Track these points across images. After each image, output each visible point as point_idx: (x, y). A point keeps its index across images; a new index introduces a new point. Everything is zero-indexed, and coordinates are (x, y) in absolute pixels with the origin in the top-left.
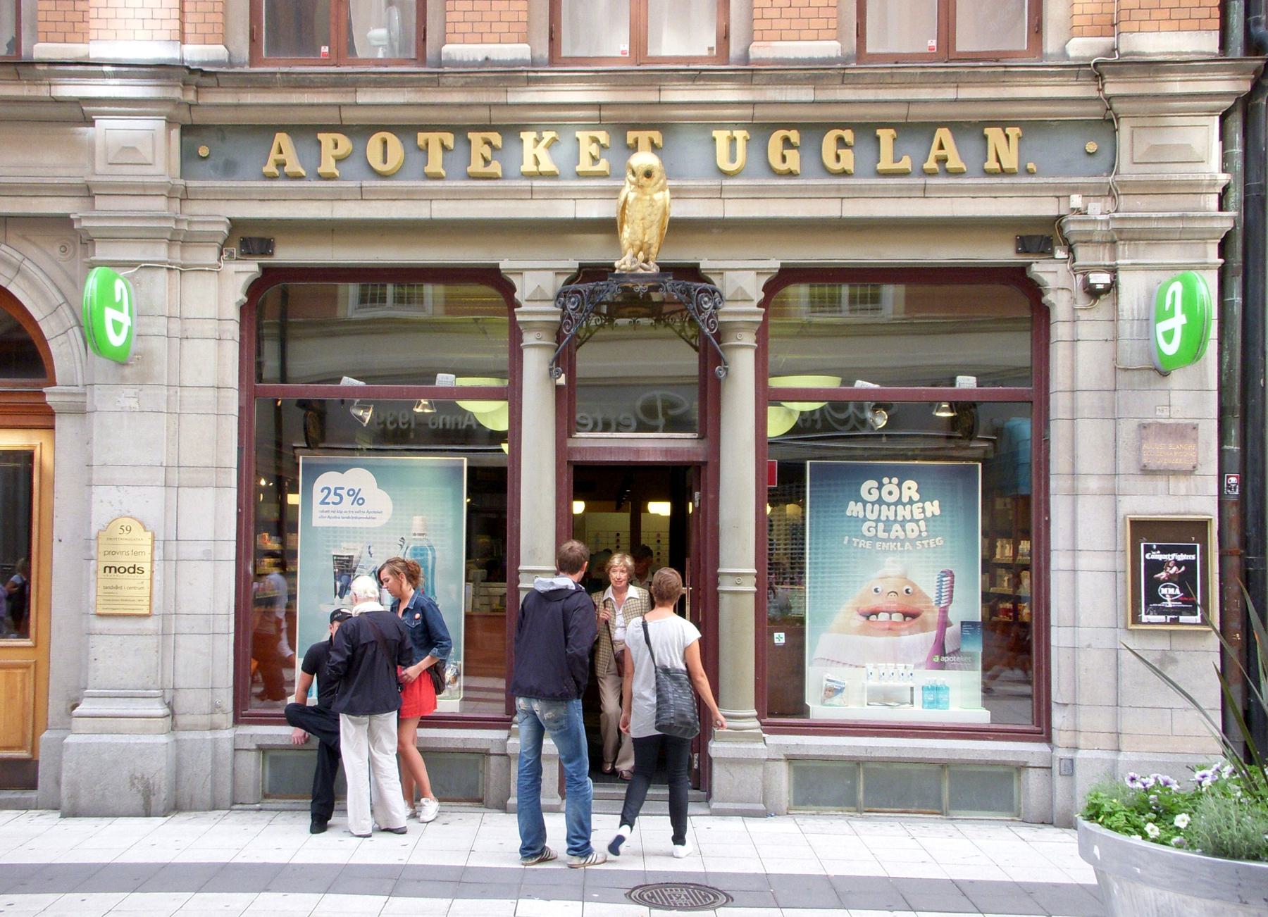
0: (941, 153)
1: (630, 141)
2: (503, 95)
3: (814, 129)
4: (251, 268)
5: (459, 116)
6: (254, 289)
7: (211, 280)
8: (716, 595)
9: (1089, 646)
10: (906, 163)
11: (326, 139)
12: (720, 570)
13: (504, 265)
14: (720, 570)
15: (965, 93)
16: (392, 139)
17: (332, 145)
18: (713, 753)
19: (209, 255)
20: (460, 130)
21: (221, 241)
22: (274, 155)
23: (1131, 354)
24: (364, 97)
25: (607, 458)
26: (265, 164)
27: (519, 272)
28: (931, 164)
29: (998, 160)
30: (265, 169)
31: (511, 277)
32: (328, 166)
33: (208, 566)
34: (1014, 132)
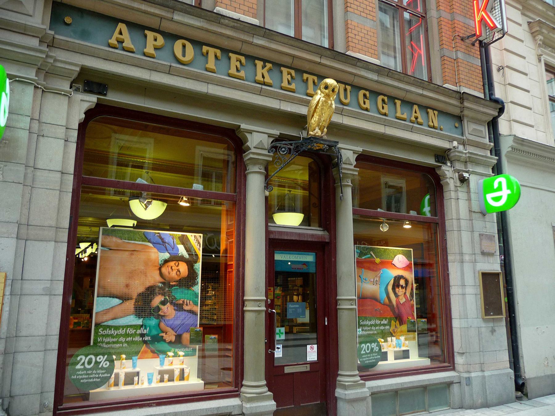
0: (120, 36)
1: (305, 78)
2: (252, 38)
3: (375, 93)
4: (93, 99)
5: (226, 43)
6: (89, 114)
7: (64, 101)
8: (336, 310)
9: (471, 327)
10: (405, 116)
11: (150, 35)
12: (338, 298)
14: (338, 298)
15: (426, 93)
16: (189, 46)
17: (152, 39)
18: (273, 403)
19: (65, 86)
20: (226, 51)
21: (74, 77)
22: (116, 34)
23: (475, 207)
24: (177, 17)
25: (286, 238)
26: (111, 38)
27: (250, 132)
28: (413, 119)
29: (433, 122)
30: (110, 41)
31: (246, 134)
32: (150, 49)
33: (47, 298)
34: (269, 65)
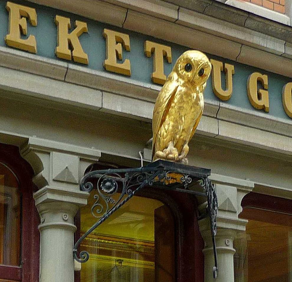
1: (148, 49)
13: (34, 140)
27: (47, 151)
31: (40, 155)
34: (81, 25)
